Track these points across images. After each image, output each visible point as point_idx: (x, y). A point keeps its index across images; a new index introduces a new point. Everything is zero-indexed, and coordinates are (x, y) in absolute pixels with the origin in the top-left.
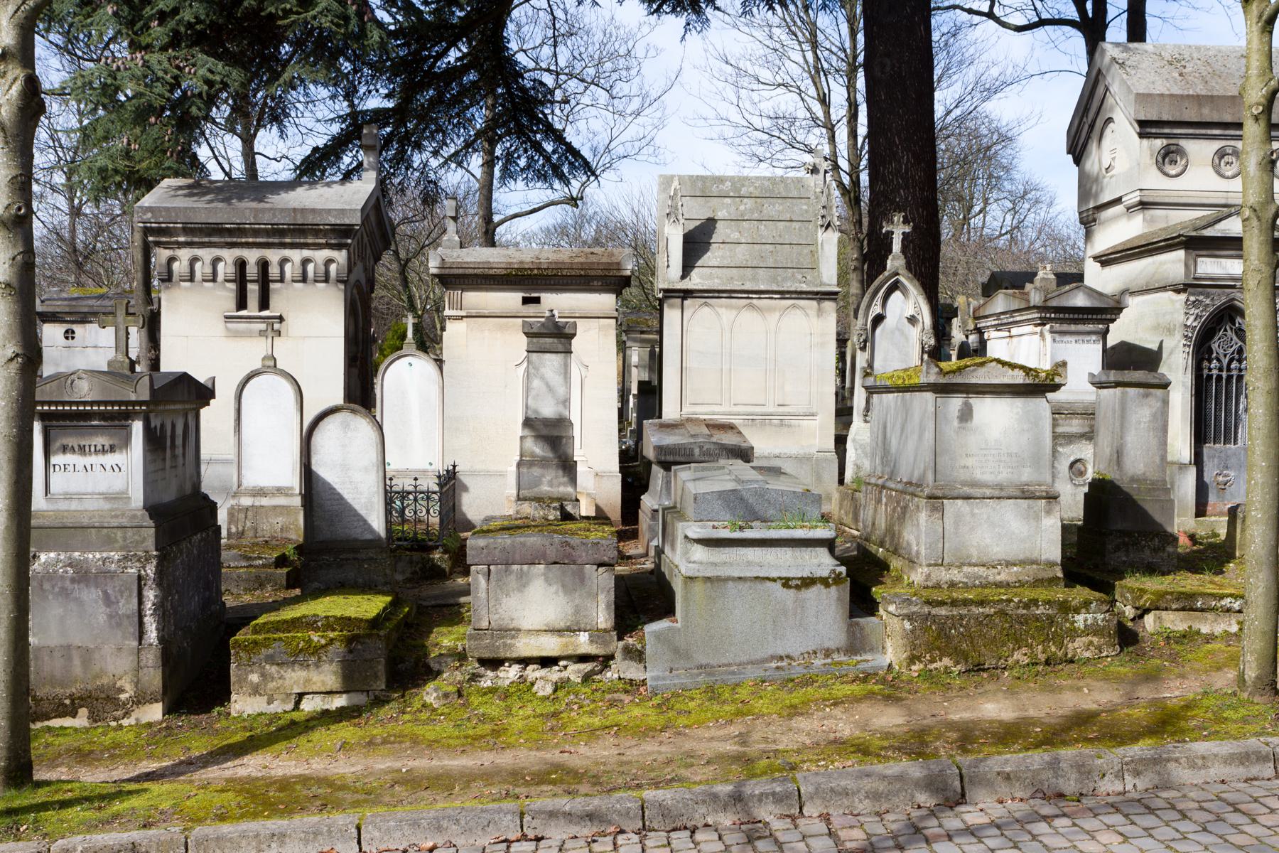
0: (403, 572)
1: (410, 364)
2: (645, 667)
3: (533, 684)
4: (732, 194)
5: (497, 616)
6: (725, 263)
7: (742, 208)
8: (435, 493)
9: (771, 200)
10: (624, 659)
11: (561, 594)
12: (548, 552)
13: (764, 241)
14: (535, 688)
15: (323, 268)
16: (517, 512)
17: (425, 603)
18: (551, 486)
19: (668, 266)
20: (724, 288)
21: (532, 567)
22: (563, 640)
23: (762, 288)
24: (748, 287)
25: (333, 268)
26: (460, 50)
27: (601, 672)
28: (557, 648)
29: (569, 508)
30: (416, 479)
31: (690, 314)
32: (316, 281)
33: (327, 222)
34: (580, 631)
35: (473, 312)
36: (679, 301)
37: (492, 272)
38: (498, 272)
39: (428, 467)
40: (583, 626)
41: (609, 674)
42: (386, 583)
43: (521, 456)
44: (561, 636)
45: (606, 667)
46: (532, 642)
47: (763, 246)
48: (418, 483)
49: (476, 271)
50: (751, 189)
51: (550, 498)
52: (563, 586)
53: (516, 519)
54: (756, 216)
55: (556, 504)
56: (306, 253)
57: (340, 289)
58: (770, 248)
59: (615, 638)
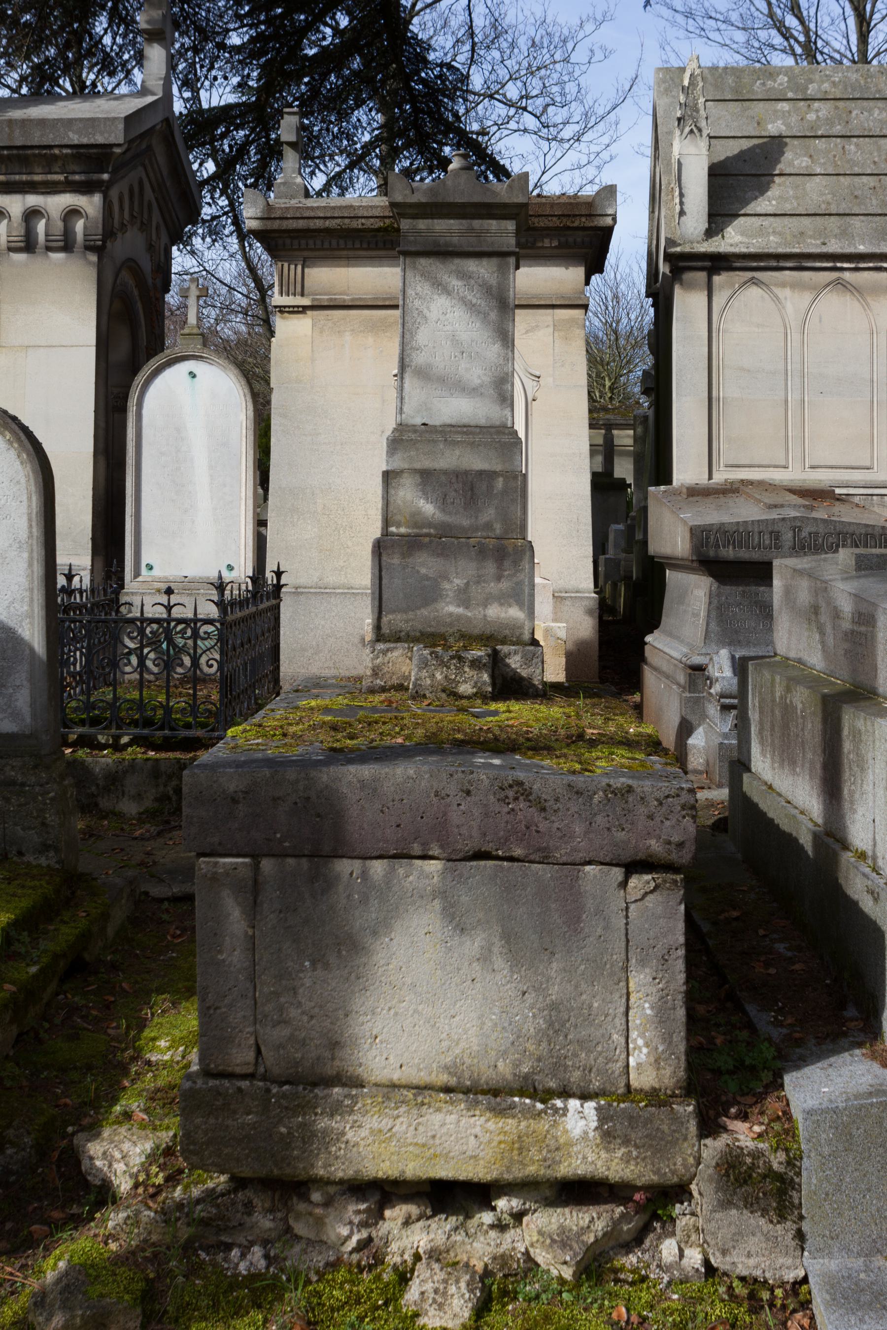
0: (138, 797)
1: (193, 375)
2: (800, 1236)
3: (404, 1277)
4: (790, 95)
5: (285, 1032)
6: (788, 208)
7: (812, 116)
8: (209, 622)
9: (865, 103)
10: (725, 1204)
11: (499, 962)
12: (455, 817)
13: (857, 170)
14: (412, 1294)
15: (60, 224)
16: (376, 672)
17: (157, 891)
18: (466, 603)
19: (682, 213)
20: (788, 250)
21: (401, 868)
22: (510, 1124)
23: (862, 248)
24: (834, 247)
25: (79, 226)
27: (637, 1241)
28: (487, 1154)
29: (515, 662)
30: (169, 591)
31: (723, 301)
32: (49, 249)
33: (66, 142)
34: (565, 1094)
35: (324, 299)
36: (702, 276)
37: (356, 224)
38: (368, 223)
40: (575, 1076)
41: (668, 1249)
42: (45, 848)
43: (387, 522)
44: (500, 1112)
45: (655, 1217)
46: (400, 1127)
47: (856, 179)
48: (174, 599)
49: (328, 223)
50: (826, 86)
51: (463, 636)
52: (507, 937)
53: (372, 691)
54: (838, 129)
55: (478, 652)
56: (33, 200)
57: (90, 263)
58: (871, 181)
59: (692, 1127)
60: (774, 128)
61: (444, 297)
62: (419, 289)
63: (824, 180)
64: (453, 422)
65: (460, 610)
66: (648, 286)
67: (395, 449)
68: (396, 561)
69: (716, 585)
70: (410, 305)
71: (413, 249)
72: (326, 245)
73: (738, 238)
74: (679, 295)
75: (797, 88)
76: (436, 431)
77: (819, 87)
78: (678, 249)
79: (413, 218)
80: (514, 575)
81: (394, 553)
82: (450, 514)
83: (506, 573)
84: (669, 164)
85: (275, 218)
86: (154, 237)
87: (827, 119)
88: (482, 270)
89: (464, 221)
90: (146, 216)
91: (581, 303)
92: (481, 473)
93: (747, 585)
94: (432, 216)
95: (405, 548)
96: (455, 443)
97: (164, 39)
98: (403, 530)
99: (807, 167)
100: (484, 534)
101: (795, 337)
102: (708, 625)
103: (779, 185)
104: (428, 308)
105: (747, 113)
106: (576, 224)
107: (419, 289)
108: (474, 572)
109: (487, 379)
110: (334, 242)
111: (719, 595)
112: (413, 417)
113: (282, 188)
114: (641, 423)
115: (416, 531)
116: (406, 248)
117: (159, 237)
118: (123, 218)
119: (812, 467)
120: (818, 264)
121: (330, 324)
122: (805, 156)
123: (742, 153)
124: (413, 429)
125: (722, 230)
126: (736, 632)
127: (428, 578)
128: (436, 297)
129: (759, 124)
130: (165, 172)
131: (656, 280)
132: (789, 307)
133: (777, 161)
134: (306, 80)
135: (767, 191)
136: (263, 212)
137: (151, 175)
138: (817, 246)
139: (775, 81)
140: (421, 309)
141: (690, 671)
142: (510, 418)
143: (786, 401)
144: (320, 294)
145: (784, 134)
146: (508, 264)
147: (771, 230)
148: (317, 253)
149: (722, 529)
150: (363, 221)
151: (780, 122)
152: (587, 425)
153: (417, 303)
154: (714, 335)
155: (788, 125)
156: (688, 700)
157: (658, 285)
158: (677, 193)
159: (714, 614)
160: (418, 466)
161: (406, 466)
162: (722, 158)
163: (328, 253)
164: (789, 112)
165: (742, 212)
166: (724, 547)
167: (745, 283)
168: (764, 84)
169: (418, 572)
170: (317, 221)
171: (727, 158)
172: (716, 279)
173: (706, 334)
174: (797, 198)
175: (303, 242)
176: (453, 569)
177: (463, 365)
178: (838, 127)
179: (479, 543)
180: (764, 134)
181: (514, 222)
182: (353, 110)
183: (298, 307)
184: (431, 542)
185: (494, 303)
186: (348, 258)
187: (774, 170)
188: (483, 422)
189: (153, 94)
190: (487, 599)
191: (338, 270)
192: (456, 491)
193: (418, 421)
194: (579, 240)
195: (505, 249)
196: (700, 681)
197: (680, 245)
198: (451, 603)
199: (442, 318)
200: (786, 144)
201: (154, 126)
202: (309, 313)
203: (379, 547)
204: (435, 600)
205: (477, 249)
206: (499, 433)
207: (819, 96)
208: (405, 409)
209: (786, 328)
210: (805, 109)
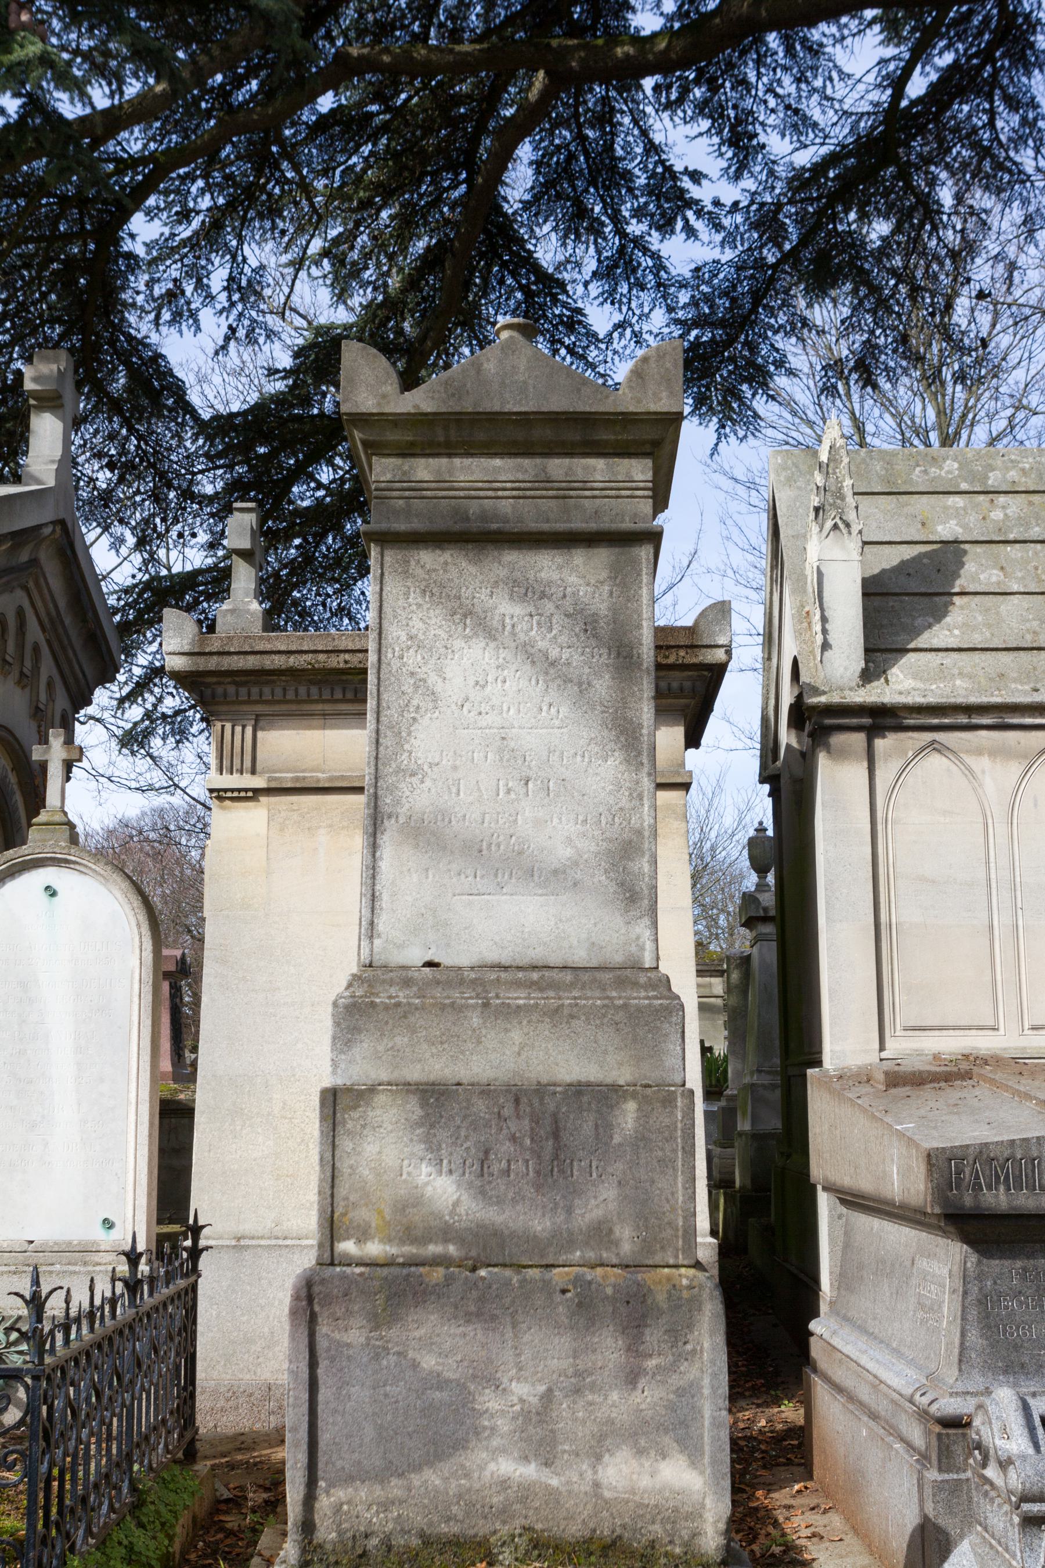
1: (51, 892)
4: (964, 486)
6: (977, 639)
7: (997, 515)
19: (826, 646)
20: (984, 699)
26: (335, 468)
31: (892, 776)
35: (287, 778)
36: (859, 739)
39: (99, 1234)
49: (292, 661)
50: (1013, 475)
60: (946, 530)
61: (478, 644)
62: (417, 624)
63: (1026, 601)
64: (504, 957)
65: (530, 1471)
66: (763, 766)
67: (355, 1030)
68: (355, 1335)
69: (973, 1258)
70: (395, 664)
71: (402, 526)
72: (290, 695)
73: (909, 683)
74: (825, 768)
75: (973, 477)
76: (462, 982)
77: (1004, 476)
78: (823, 699)
79: (403, 455)
80: (672, 1368)
81: (349, 1313)
82: (500, 1201)
83: (651, 1363)
84: (802, 578)
85: (211, 654)
86: (43, 697)
87: (1020, 518)
88: (573, 579)
89: (526, 462)
90: (28, 663)
91: (679, 780)
92: (578, 1090)
93: (1030, 1256)
94: (449, 449)
95: (380, 1299)
96: (509, 1013)
97: (62, 406)
98: (374, 1249)
99: (998, 583)
100: (591, 1255)
101: (999, 829)
102: (963, 1335)
103: (962, 608)
104: (440, 672)
105: (905, 510)
106: (671, 660)
107: (417, 624)
108: (566, 1363)
109: (588, 847)
110: (302, 690)
111: (980, 1277)
112: (401, 947)
113: (229, 617)
114: (737, 967)
115: (410, 1249)
116: (384, 526)
117: (51, 698)
118: (38, 701)
119: (1034, 1028)
120: (1028, 721)
121: (295, 816)
122: (994, 568)
123: (903, 564)
124: (403, 976)
125: (884, 672)
126: (1017, 1348)
127: (441, 1383)
128: (458, 643)
129: (923, 524)
130: (62, 603)
131: (775, 757)
132: (989, 785)
133: (956, 575)
134: (297, 541)
135: (945, 616)
136: (191, 644)
137: (39, 604)
138: (1025, 693)
139: (941, 468)
140: (421, 673)
141: (938, 1429)
142: (649, 946)
143: (991, 927)
144: (280, 771)
145: (961, 538)
146: (635, 563)
147: (956, 671)
148: (277, 708)
149: (983, 1154)
150: (347, 656)
151: (953, 522)
152: (693, 969)
153: (412, 659)
154: (880, 828)
155: (965, 527)
156: (939, 1487)
157: (779, 764)
158: (818, 616)
159: (973, 1313)
160: (414, 1073)
161: (384, 1076)
162: (876, 571)
163: (294, 707)
164: (964, 509)
165: (912, 646)
166: (990, 1188)
167: (923, 749)
168: (925, 472)
169: (415, 1365)
170: (276, 657)
171: (884, 571)
172: (879, 743)
173: (869, 826)
174: (989, 626)
175: (255, 690)
176: (508, 1355)
177: (529, 811)
178: (1037, 529)
179: (577, 1280)
180: (932, 538)
181: (649, 463)
182: (356, 580)
183: (246, 790)
184: (449, 1280)
185: (603, 657)
186: (324, 715)
187: (953, 587)
188: (580, 956)
189: (39, 482)
190: (601, 1438)
191: (309, 733)
192: (513, 1139)
193: (415, 955)
194: (675, 685)
195: (627, 525)
196: (958, 1449)
197: (824, 693)
198: (503, 1451)
199: (475, 694)
200: (965, 552)
201: (39, 527)
202: (263, 799)
203: (310, 1299)
204: (460, 1445)
205: (561, 526)
206: (621, 983)
207: (1004, 488)
208: (381, 926)
209: (985, 816)
210: (987, 505)
